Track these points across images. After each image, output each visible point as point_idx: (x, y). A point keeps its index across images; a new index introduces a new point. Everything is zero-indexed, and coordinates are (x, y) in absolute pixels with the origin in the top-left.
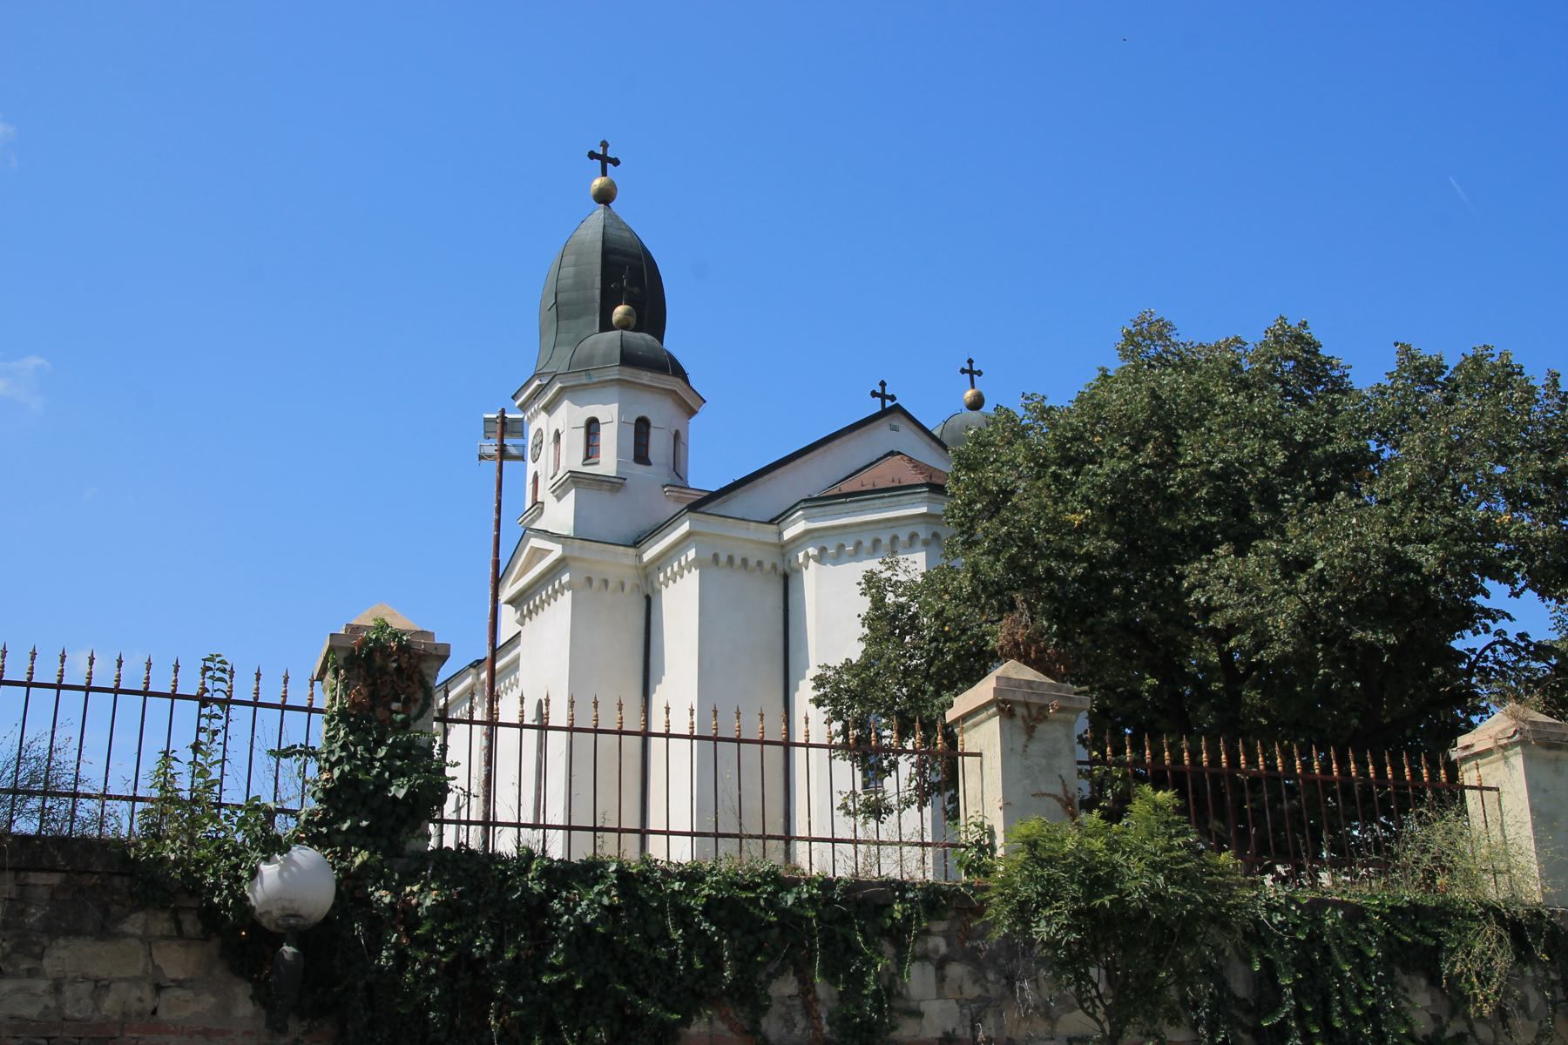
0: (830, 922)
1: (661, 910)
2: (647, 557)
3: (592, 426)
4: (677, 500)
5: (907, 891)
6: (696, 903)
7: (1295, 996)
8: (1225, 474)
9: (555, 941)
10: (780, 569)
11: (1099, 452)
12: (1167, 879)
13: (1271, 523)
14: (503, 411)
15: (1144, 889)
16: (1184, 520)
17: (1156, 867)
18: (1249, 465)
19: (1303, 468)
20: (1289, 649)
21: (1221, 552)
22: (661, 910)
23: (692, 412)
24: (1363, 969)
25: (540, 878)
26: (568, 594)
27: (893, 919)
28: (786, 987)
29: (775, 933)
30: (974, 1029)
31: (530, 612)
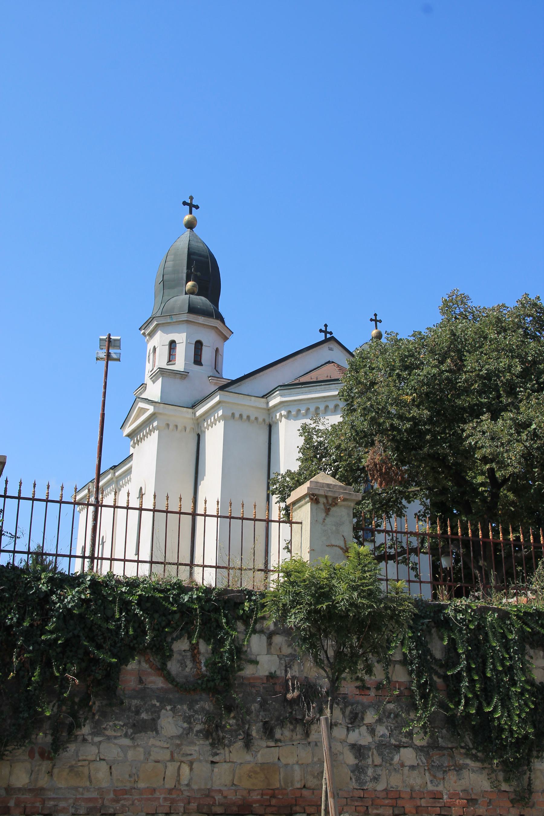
0: (209, 611)
1: (113, 601)
2: (198, 413)
3: (172, 344)
4: (216, 384)
5: (252, 595)
6: (134, 599)
7: (467, 659)
8: (488, 377)
9: (52, 617)
10: (267, 422)
11: (423, 363)
12: (359, 595)
13: (512, 403)
14: (110, 335)
15: (347, 600)
16: (463, 402)
17: (354, 589)
18: (503, 372)
19: (532, 374)
20: (516, 470)
21: (483, 418)
22: (113, 601)
23: (226, 339)
24: (506, 646)
25: (47, 583)
26: (157, 432)
27: (244, 610)
28: (181, 645)
29: (177, 616)
30: (286, 672)
31: (138, 441)
